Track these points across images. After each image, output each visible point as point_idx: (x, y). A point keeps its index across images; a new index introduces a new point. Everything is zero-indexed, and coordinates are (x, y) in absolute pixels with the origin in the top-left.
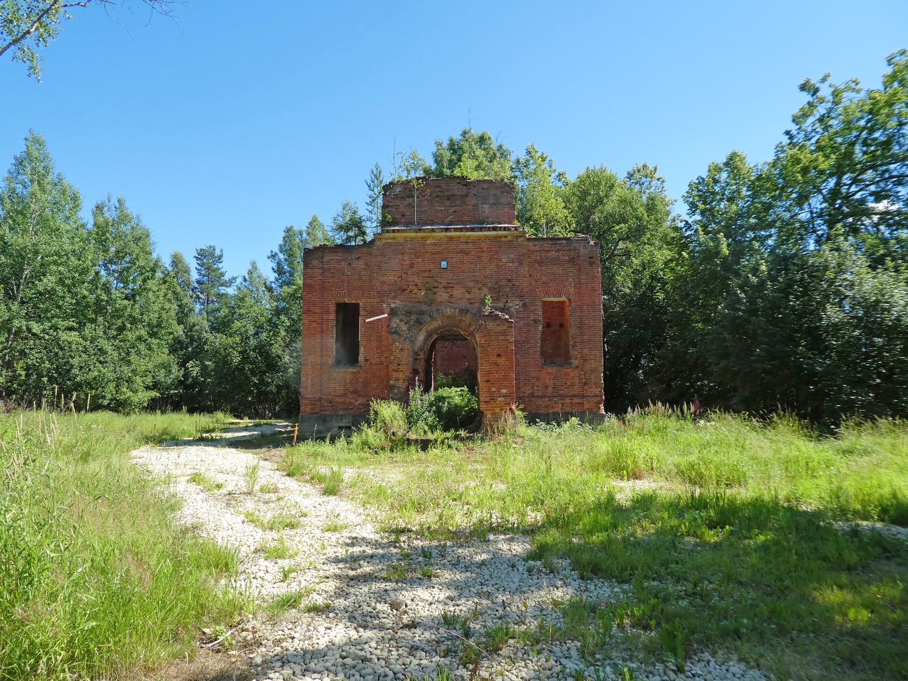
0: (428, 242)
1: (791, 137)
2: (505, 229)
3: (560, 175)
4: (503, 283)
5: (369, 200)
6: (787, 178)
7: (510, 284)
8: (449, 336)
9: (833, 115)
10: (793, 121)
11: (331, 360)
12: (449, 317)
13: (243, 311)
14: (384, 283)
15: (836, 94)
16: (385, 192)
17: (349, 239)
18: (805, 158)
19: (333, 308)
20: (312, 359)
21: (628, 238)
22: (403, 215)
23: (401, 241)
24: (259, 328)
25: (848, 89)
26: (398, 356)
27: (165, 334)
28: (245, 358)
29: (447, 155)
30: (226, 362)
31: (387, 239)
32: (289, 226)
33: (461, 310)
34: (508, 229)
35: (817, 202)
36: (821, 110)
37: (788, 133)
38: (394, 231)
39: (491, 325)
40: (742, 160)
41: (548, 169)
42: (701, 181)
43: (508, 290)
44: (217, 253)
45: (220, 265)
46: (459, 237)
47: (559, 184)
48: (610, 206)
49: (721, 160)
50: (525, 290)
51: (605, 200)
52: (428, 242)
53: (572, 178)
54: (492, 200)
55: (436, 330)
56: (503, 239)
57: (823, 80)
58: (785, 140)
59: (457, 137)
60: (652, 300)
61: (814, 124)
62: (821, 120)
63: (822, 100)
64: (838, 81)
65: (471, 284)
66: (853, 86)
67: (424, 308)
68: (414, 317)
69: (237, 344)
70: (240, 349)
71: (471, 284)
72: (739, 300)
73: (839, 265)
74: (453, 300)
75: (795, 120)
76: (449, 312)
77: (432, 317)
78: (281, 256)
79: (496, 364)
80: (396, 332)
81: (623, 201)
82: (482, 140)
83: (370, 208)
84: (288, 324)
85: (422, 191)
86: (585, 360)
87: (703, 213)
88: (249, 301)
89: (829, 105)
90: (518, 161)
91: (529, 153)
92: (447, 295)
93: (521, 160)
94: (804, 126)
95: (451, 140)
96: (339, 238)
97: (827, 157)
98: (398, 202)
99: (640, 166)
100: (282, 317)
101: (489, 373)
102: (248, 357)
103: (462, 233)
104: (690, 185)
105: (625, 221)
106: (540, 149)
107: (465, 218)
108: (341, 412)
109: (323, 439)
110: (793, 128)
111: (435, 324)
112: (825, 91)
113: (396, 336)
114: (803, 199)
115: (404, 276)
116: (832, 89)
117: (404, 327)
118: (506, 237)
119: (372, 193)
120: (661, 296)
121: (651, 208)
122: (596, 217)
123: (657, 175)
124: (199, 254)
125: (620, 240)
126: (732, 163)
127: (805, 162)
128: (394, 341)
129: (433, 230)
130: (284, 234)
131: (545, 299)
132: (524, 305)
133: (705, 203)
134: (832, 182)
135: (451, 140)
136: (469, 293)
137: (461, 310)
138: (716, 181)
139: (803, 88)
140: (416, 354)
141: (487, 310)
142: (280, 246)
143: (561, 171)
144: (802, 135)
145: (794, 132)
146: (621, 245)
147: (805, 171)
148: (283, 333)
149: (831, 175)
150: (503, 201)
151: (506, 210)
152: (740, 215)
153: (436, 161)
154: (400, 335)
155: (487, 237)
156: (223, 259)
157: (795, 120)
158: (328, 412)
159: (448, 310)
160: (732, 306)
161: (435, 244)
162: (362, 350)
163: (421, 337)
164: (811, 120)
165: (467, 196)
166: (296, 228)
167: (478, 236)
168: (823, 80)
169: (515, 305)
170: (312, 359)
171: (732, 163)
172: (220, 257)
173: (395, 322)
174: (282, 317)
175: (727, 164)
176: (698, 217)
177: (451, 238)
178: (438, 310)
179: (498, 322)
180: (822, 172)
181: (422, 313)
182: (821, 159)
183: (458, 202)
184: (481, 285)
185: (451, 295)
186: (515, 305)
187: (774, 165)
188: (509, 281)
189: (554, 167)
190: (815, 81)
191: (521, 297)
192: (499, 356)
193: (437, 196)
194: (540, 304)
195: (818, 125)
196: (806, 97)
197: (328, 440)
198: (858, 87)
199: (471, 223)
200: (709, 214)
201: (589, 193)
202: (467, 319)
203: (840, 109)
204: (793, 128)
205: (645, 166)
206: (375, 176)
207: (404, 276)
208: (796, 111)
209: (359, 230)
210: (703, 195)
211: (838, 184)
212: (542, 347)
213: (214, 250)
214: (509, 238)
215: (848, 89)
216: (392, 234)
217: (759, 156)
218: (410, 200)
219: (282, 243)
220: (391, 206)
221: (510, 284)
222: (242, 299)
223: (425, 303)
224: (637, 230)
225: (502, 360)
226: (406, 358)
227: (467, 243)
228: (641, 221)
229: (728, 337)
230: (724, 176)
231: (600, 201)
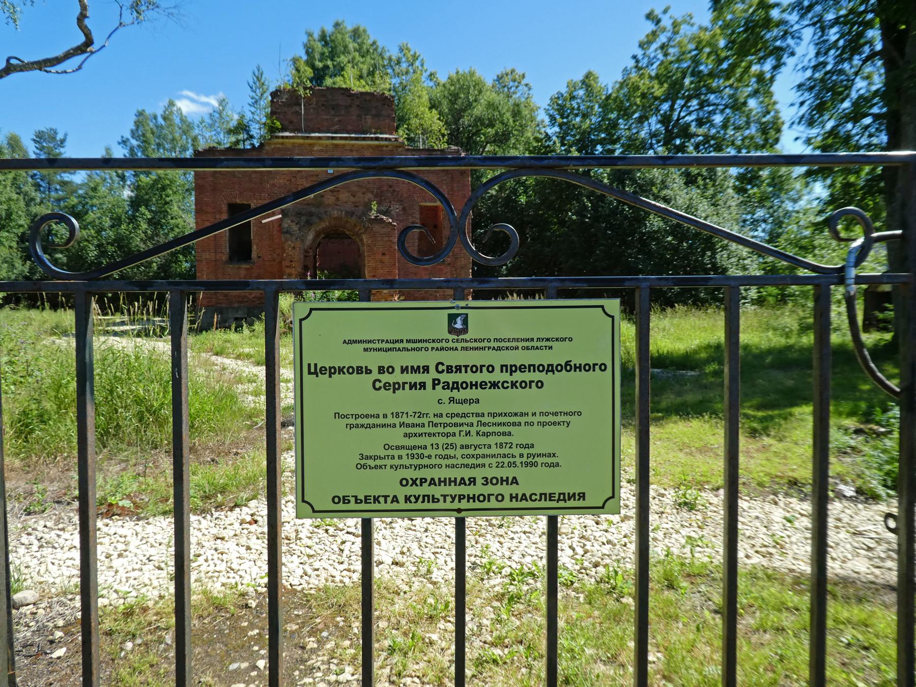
0: (315, 148)
1: (637, 61)
2: (386, 139)
3: (431, 75)
4: (385, 188)
5: (251, 101)
6: (625, 103)
7: (391, 190)
8: (334, 234)
9: (672, 43)
10: (640, 46)
11: (225, 258)
12: (335, 219)
13: (95, 201)
14: (273, 185)
15: (675, 25)
16: (273, 98)
17: (237, 142)
18: (644, 84)
19: (225, 208)
20: (206, 255)
21: (494, 141)
22: (291, 122)
23: (289, 146)
24: (117, 222)
25: (684, 22)
26: (291, 253)
27: (14, 227)
28: (103, 253)
29: (319, 46)
30: (81, 257)
31: (276, 144)
32: (140, 109)
33: (347, 213)
34: (390, 139)
35: (654, 124)
36: (663, 39)
37: (634, 57)
38: (283, 137)
39: (376, 227)
40: (596, 79)
41: (420, 68)
42: (560, 95)
43: (389, 194)
44: (60, 136)
45: (62, 150)
46: (344, 145)
47: (431, 84)
48: (479, 110)
49: (579, 77)
50: (405, 195)
51: (474, 104)
52: (315, 148)
53: (443, 79)
54: (374, 112)
55: (323, 230)
56: (385, 149)
57: (665, 11)
58: (632, 63)
59: (329, 29)
60: (516, 202)
61: (656, 50)
62: (663, 47)
63: (664, 30)
64: (677, 13)
65: (355, 189)
66: (688, 20)
67: (313, 209)
68: (304, 218)
69: (93, 237)
70: (96, 242)
71: (355, 189)
72: (587, 207)
73: (663, 182)
74: (339, 203)
75: (641, 45)
76: (335, 213)
77: (320, 219)
78: (134, 142)
79: (382, 262)
80: (287, 232)
81: (491, 105)
82: (356, 34)
83: (253, 109)
84: (149, 217)
85: (308, 100)
86: (456, 258)
87: (560, 126)
88: (103, 190)
89: (669, 34)
90: (390, 59)
91: (401, 50)
92: (334, 198)
93: (394, 58)
94: (648, 52)
95: (323, 32)
96: (227, 141)
97: (661, 84)
98: (286, 109)
99: (509, 70)
100: (143, 209)
101: (375, 269)
102: (106, 252)
103: (347, 142)
104: (551, 99)
105: (491, 125)
106: (414, 48)
107: (350, 128)
108: (236, 305)
109: (229, 328)
110: (639, 53)
111: (323, 225)
112: (666, 22)
113: (288, 236)
114: (642, 120)
115: (293, 180)
116: (672, 21)
117: (295, 228)
118: (387, 146)
119: (253, 94)
120: (523, 199)
121: (516, 114)
122: (466, 120)
123: (524, 82)
124: (37, 137)
125: (487, 143)
126: (588, 82)
127: (643, 88)
128: (287, 240)
129: (320, 138)
130: (134, 118)
131: (423, 204)
132: (404, 209)
133: (562, 117)
134: (665, 107)
135: (323, 32)
136: (354, 196)
137: (347, 213)
138: (573, 98)
139: (649, 16)
140: (306, 251)
141: (373, 214)
142: (132, 131)
143: (433, 71)
144: (646, 60)
145: (640, 57)
146: (489, 148)
147: (644, 96)
148: (144, 226)
149: (665, 100)
150: (384, 113)
151: (387, 121)
152: (592, 130)
153: (307, 53)
154: (291, 234)
155: (370, 146)
156: (66, 144)
157: (641, 45)
158: (224, 305)
159: (335, 212)
160: (581, 212)
161: (321, 151)
162: (254, 247)
163: (311, 236)
164: (654, 46)
165: (350, 106)
166: (149, 111)
167: (359, 145)
168: (665, 11)
169: (396, 208)
170: (206, 255)
171: (588, 82)
172: (63, 141)
173: (287, 223)
174: (143, 209)
175: (583, 82)
176: (557, 129)
177: (337, 145)
178: (325, 212)
179: (383, 225)
180: (656, 98)
181: (311, 214)
182: (657, 87)
183: (343, 112)
184: (364, 190)
185: (338, 199)
186: (396, 208)
187: (622, 85)
188: (390, 186)
189: (425, 68)
190: (658, 12)
191: (401, 201)
192: (383, 254)
193: (323, 105)
194: (418, 208)
195: (659, 51)
196: (650, 27)
197: (233, 328)
198: (692, 21)
199: (355, 133)
200: (565, 129)
201: (456, 100)
202: (353, 220)
203: (678, 38)
204: (639, 53)
205: (513, 71)
206: (257, 78)
207: (293, 180)
208: (642, 37)
209: (248, 134)
210: (561, 109)
211: (672, 109)
212: (419, 245)
213: (56, 133)
214: (390, 148)
215: (684, 22)
216: (281, 140)
217: (608, 81)
218: (297, 108)
219: (134, 128)
220: (279, 113)
221: (391, 190)
222: (94, 189)
223: (314, 205)
224: (503, 134)
225: (386, 259)
226: (297, 255)
227: (351, 151)
228: (509, 122)
229: (575, 239)
230: (581, 93)
231: (470, 105)
